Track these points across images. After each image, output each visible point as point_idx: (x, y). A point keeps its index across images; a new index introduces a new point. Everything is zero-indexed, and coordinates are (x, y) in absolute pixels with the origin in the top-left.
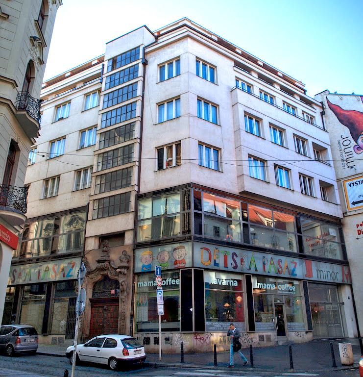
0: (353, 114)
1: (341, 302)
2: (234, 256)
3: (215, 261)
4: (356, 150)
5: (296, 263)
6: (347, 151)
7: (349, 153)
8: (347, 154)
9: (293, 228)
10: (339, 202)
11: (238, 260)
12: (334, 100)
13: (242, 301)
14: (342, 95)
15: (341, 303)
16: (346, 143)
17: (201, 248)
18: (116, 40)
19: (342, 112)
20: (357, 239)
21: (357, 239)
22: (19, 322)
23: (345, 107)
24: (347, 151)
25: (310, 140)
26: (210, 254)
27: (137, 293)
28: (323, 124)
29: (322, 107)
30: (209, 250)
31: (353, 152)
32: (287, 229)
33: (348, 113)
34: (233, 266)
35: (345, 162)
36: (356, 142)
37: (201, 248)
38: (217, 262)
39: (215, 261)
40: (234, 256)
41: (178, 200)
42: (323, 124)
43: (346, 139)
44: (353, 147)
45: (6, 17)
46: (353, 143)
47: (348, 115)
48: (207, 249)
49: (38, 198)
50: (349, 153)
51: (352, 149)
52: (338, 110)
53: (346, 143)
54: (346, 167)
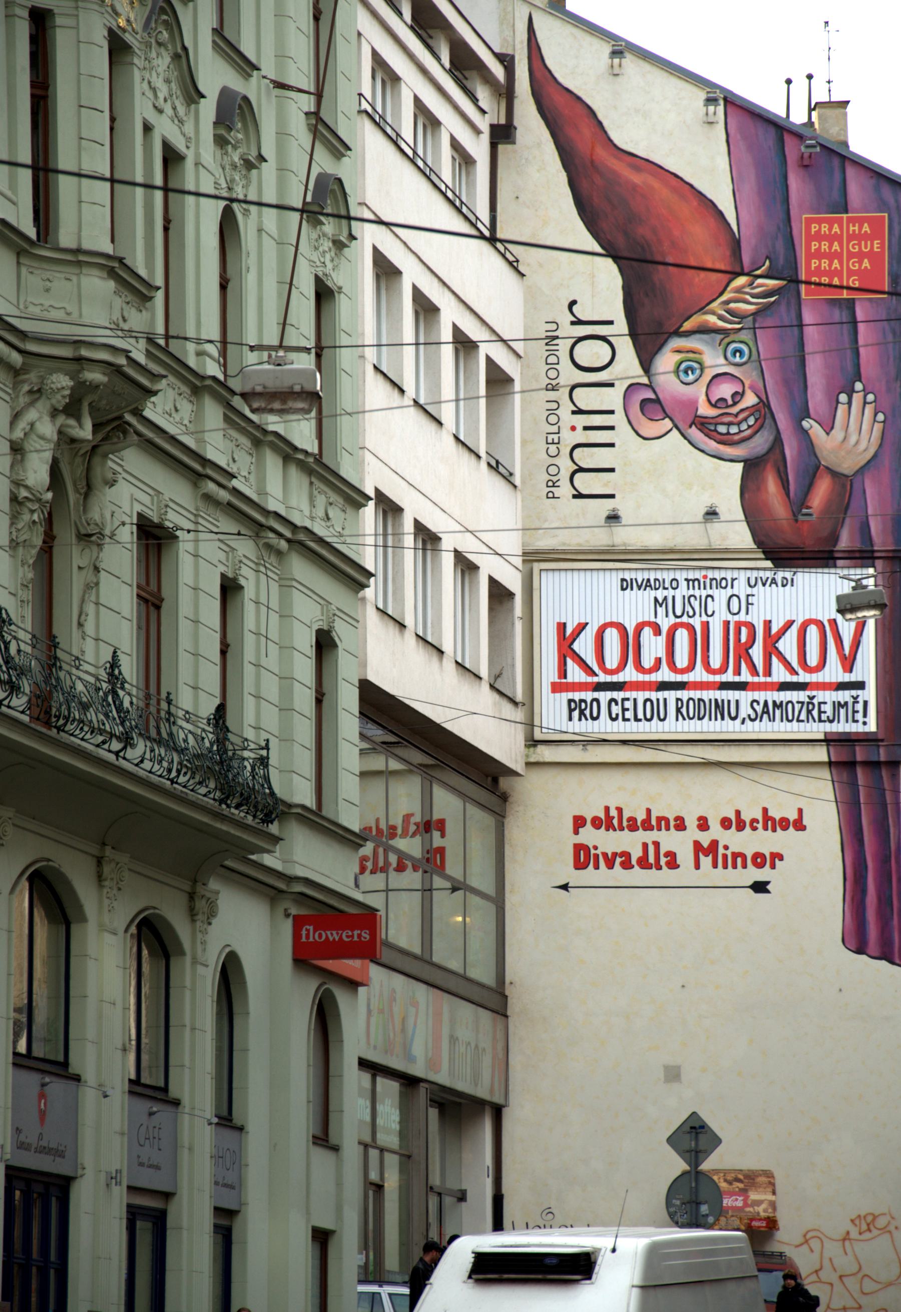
0: (662, 191)
1: (452, 1184)
4: (635, 408)
6: (586, 398)
7: (597, 420)
8: (582, 421)
10: (519, 697)
12: (576, 65)
15: (451, 1193)
16: (592, 353)
18: (379, 412)
19: (601, 153)
20: (565, 887)
21: (565, 887)
23: (627, 133)
24: (586, 398)
25: (448, 543)
27: (765, 360)
28: (308, 1165)
29: (506, 93)
31: (618, 419)
33: (636, 178)
35: (567, 467)
36: (646, 365)
42: (308, 1165)
43: (592, 330)
44: (621, 388)
46: (628, 363)
47: (635, 187)
50: (597, 420)
51: (613, 398)
52: (583, 137)
53: (592, 353)
54: (565, 490)
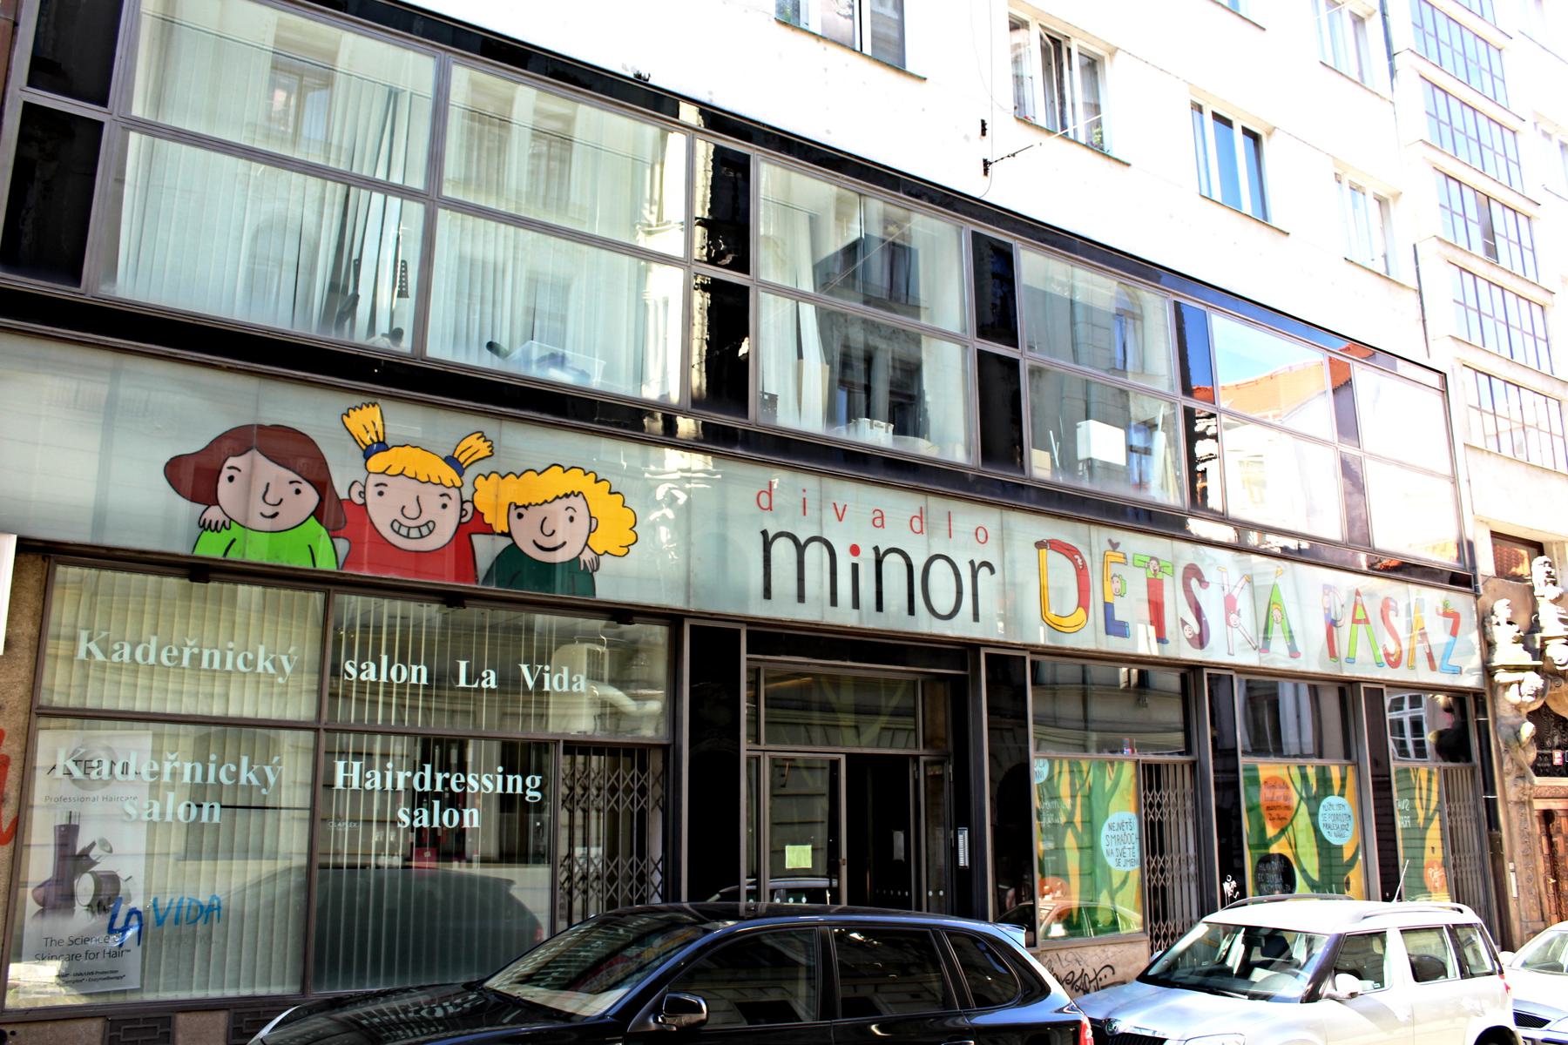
2: (1194, 582)
3: (1108, 608)
5: (1543, 640)
9: (763, 180)
11: (1211, 601)
13: (1223, 880)
14: (1384, 15)
17: (1040, 545)
22: (772, 707)
26: (1082, 573)
30: (1078, 553)
32: (712, 148)
34: (1188, 634)
37: (1040, 545)
38: (1118, 616)
39: (1108, 608)
40: (1194, 582)
41: (263, 172)
45: (1562, 621)
48: (1069, 551)
49: (1078, 298)
